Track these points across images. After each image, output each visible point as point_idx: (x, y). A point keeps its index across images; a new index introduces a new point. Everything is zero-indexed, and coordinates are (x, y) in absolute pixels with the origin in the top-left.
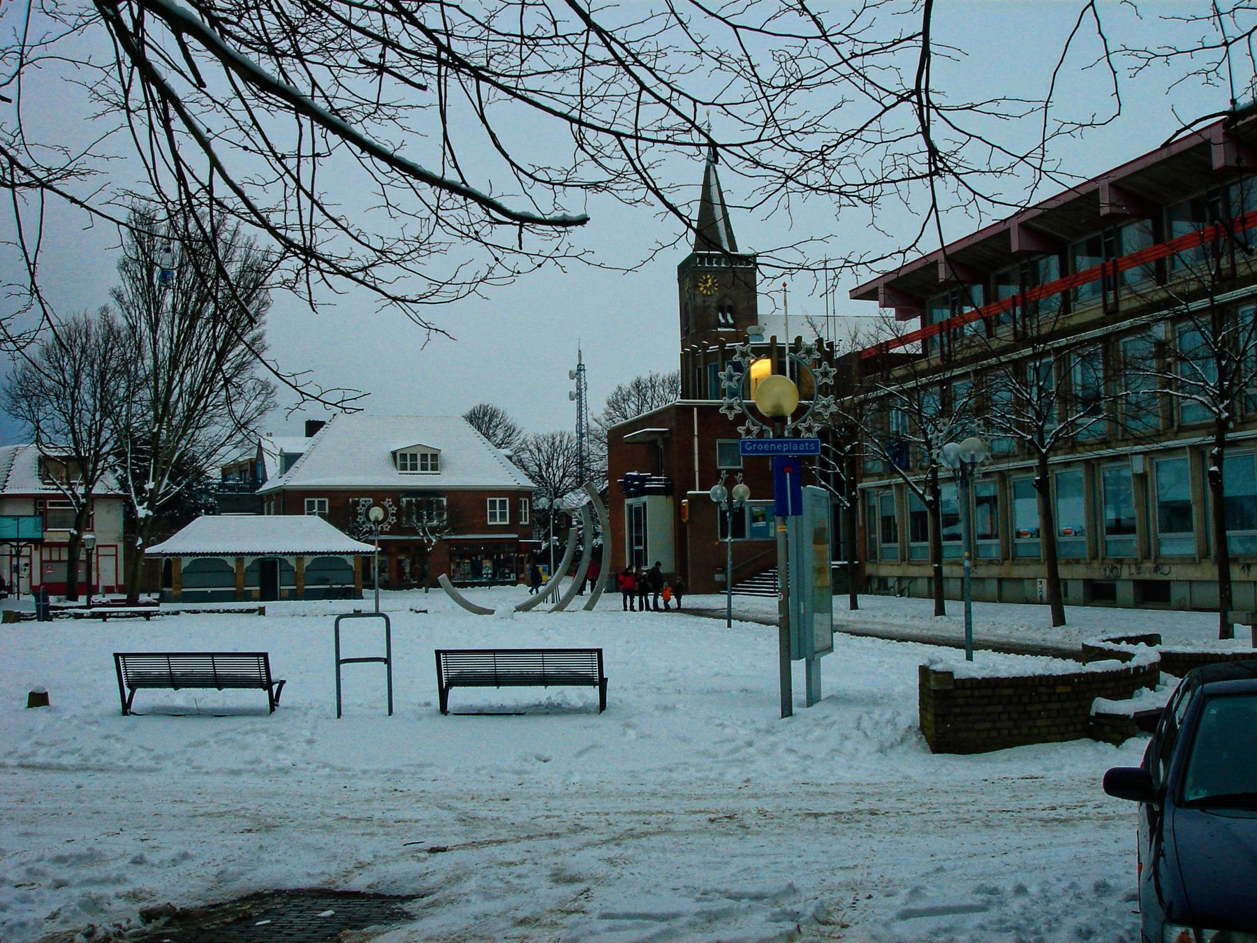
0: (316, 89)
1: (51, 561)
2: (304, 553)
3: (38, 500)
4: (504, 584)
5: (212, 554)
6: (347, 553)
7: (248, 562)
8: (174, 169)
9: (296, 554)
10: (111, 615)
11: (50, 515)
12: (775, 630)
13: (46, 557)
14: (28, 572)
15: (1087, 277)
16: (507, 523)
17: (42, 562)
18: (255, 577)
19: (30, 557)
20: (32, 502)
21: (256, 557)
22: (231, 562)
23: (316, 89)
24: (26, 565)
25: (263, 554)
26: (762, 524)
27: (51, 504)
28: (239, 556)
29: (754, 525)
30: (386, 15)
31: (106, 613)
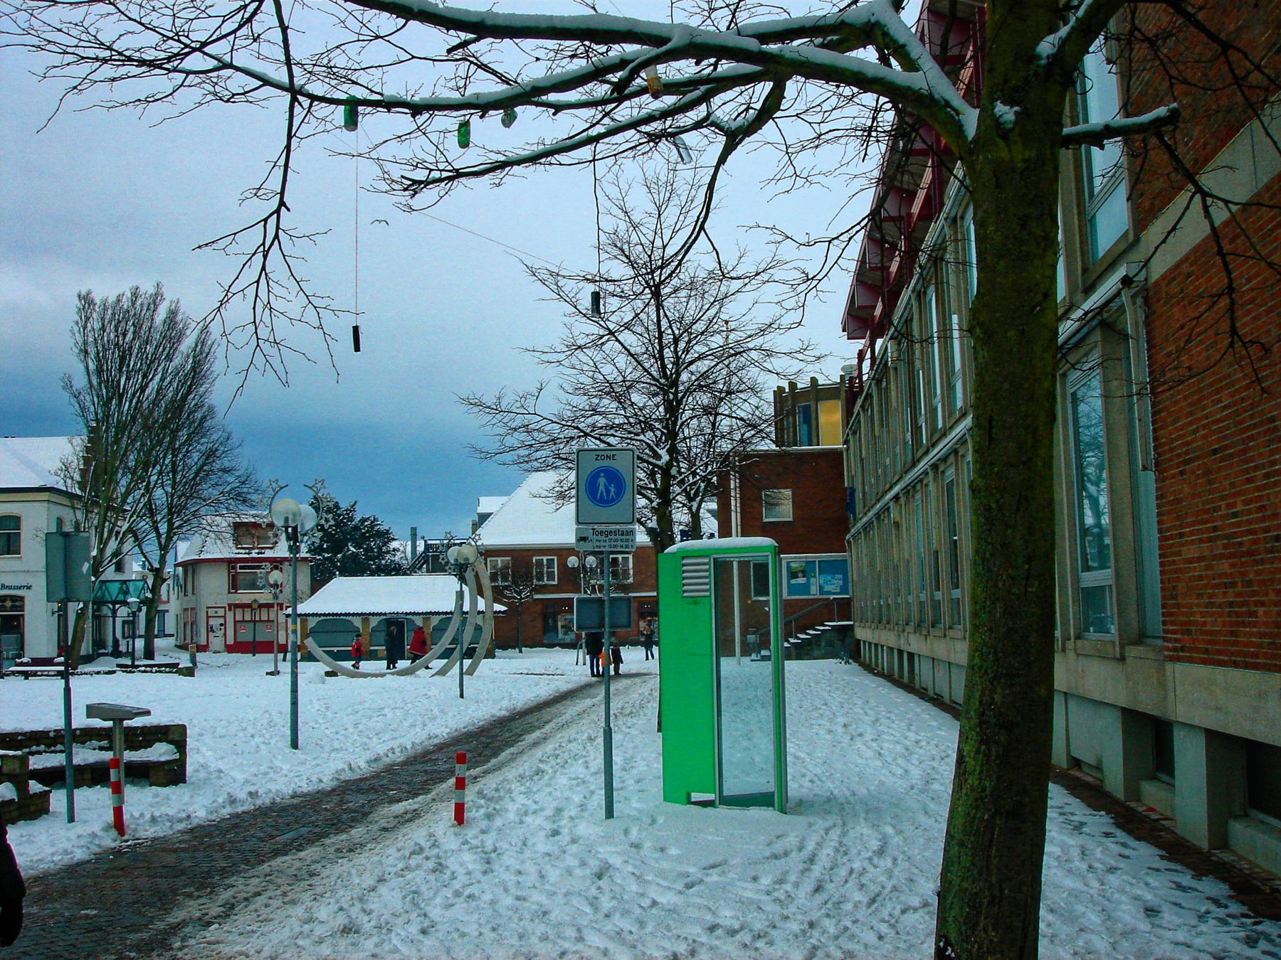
0: (1230, 205)
1: (243, 621)
2: (309, 615)
3: (231, 563)
4: (551, 646)
5: (333, 615)
6: (354, 615)
7: (374, 622)
8: (134, 70)
9: (362, 614)
10: (35, 674)
11: (240, 577)
12: (60, 724)
13: (239, 618)
14: (223, 631)
15: (889, 54)
16: (556, 583)
17: (235, 622)
18: (382, 636)
19: (224, 617)
20: (226, 564)
21: (319, 619)
22: (357, 622)
23: (1230, 205)
24: (221, 625)
25: (385, 614)
26: (801, 580)
27: (241, 568)
28: (365, 617)
29: (793, 581)
30: (1223, 56)
31: (37, 671)
